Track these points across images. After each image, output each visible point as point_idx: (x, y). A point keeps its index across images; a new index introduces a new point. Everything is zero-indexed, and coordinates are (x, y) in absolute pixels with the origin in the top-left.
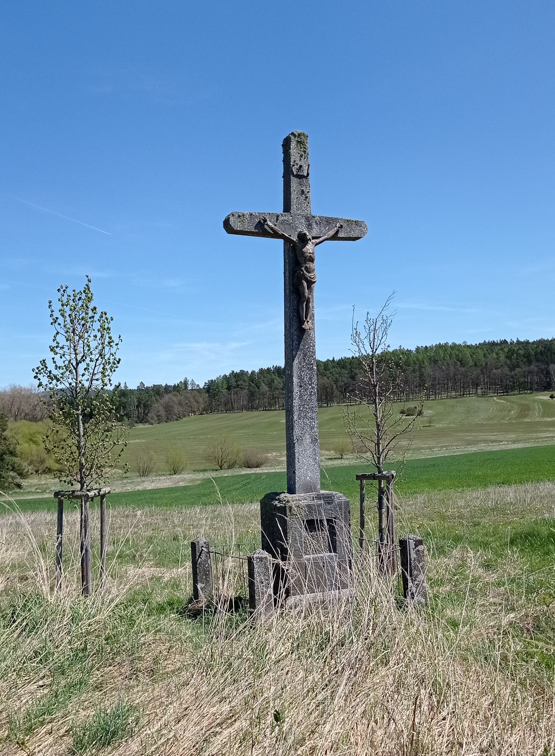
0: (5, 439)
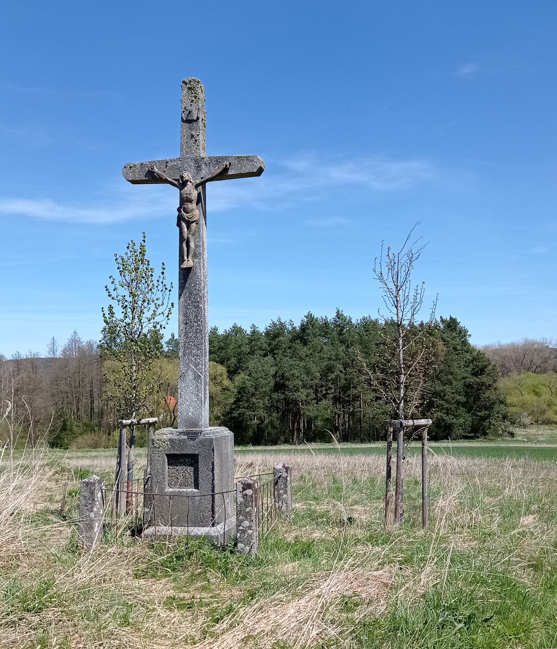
0: (495, 389)
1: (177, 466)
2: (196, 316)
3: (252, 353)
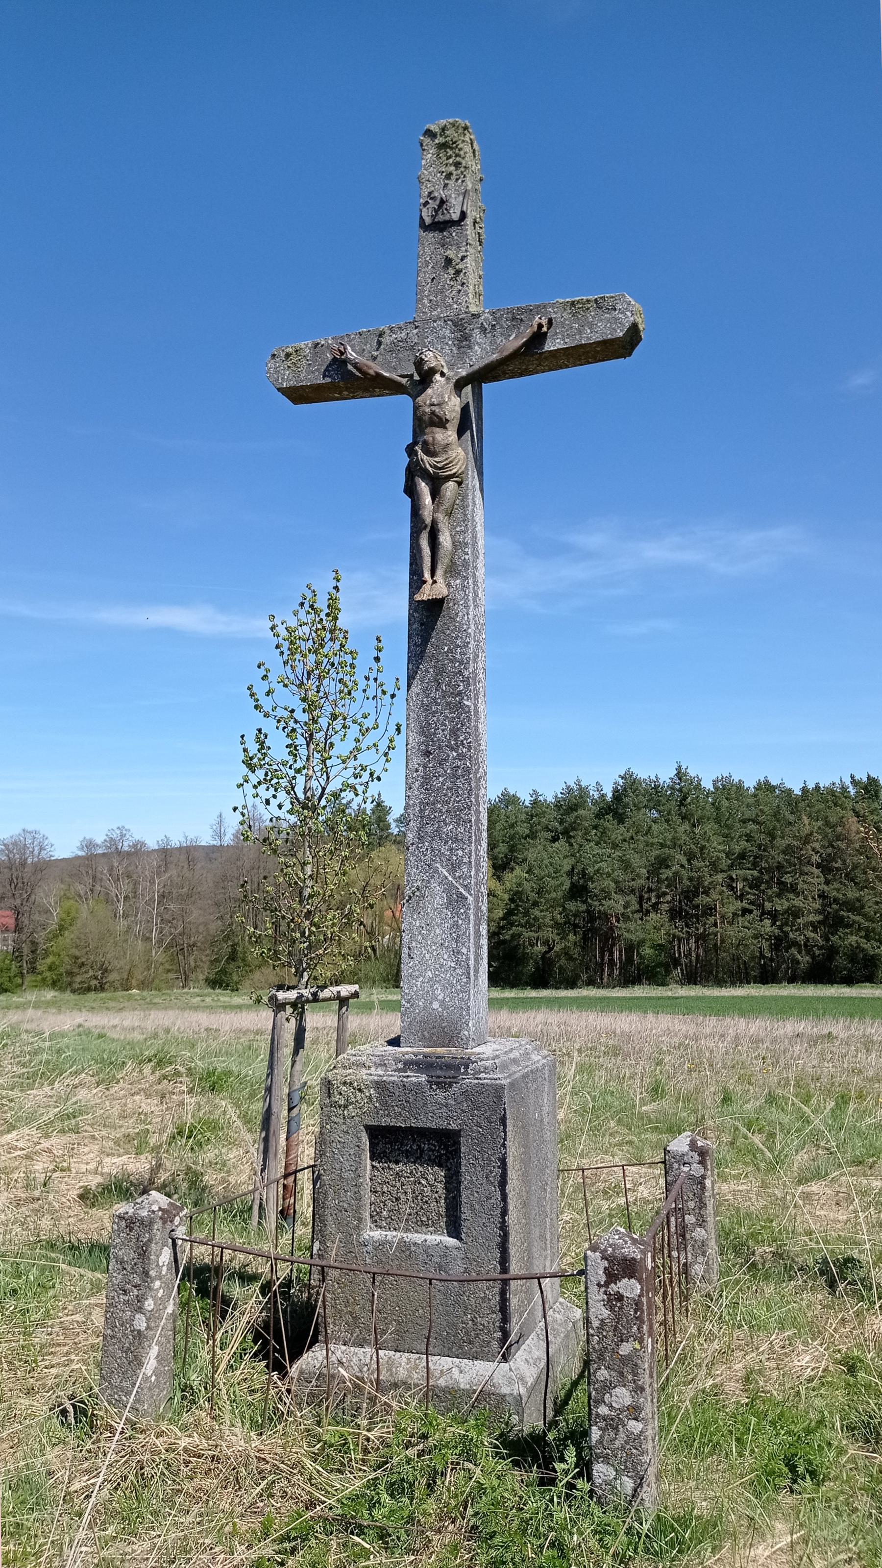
1: (397, 1163)
2: (454, 732)
3: (533, 835)
